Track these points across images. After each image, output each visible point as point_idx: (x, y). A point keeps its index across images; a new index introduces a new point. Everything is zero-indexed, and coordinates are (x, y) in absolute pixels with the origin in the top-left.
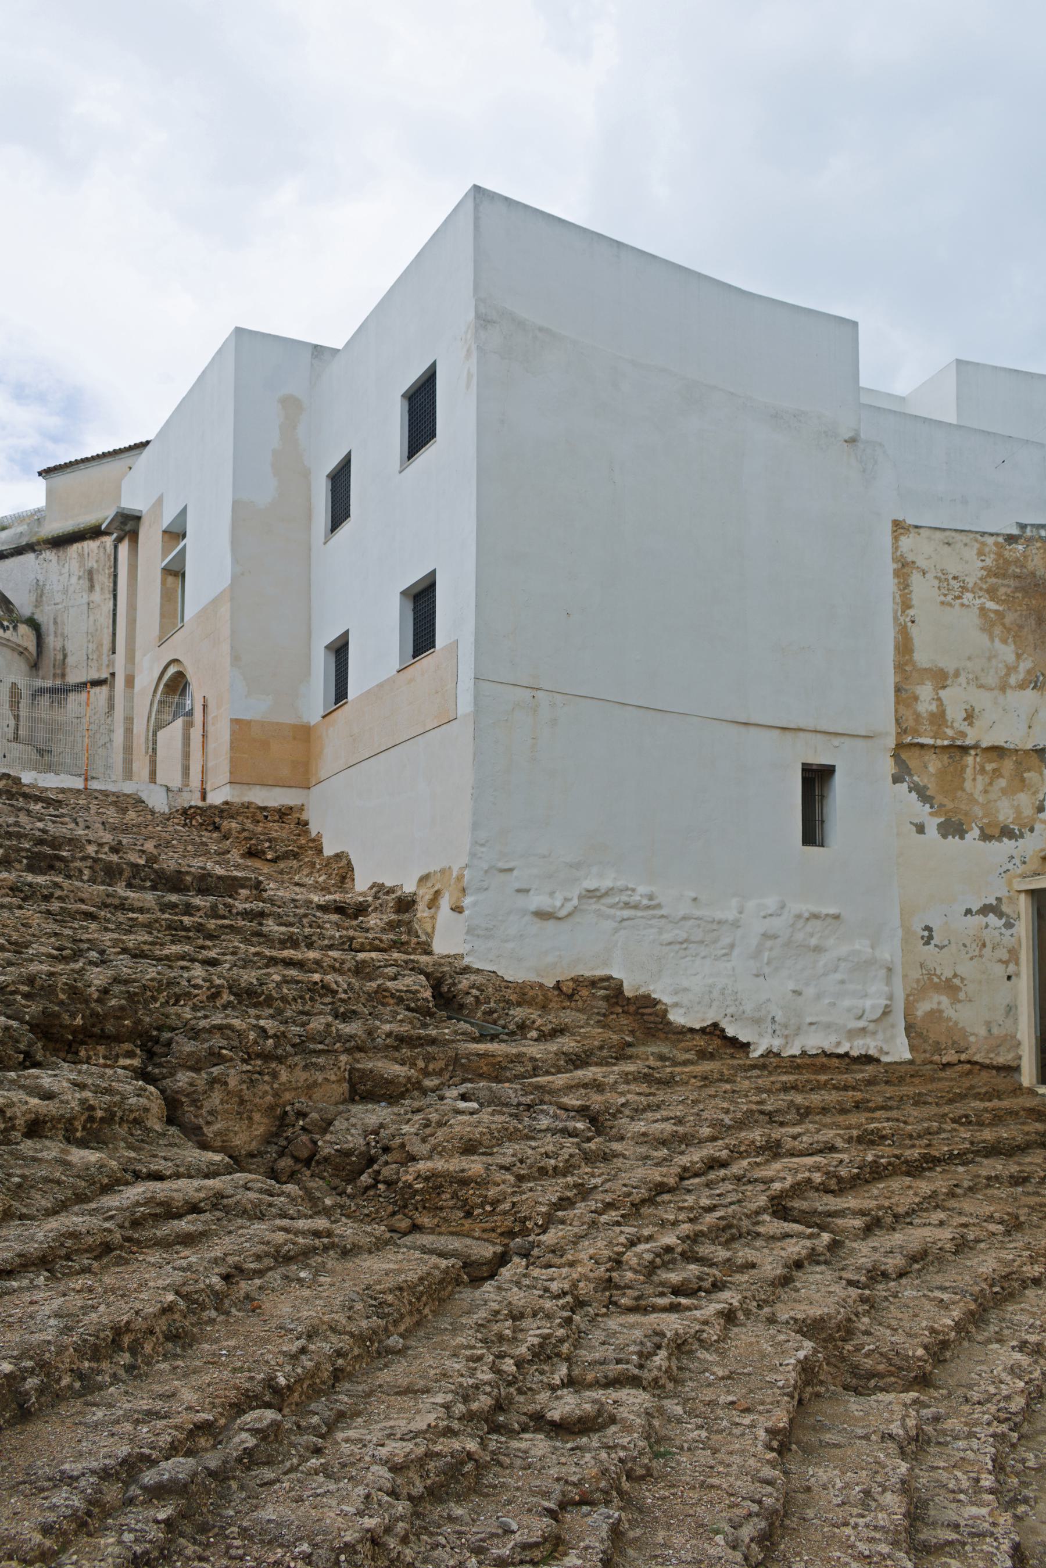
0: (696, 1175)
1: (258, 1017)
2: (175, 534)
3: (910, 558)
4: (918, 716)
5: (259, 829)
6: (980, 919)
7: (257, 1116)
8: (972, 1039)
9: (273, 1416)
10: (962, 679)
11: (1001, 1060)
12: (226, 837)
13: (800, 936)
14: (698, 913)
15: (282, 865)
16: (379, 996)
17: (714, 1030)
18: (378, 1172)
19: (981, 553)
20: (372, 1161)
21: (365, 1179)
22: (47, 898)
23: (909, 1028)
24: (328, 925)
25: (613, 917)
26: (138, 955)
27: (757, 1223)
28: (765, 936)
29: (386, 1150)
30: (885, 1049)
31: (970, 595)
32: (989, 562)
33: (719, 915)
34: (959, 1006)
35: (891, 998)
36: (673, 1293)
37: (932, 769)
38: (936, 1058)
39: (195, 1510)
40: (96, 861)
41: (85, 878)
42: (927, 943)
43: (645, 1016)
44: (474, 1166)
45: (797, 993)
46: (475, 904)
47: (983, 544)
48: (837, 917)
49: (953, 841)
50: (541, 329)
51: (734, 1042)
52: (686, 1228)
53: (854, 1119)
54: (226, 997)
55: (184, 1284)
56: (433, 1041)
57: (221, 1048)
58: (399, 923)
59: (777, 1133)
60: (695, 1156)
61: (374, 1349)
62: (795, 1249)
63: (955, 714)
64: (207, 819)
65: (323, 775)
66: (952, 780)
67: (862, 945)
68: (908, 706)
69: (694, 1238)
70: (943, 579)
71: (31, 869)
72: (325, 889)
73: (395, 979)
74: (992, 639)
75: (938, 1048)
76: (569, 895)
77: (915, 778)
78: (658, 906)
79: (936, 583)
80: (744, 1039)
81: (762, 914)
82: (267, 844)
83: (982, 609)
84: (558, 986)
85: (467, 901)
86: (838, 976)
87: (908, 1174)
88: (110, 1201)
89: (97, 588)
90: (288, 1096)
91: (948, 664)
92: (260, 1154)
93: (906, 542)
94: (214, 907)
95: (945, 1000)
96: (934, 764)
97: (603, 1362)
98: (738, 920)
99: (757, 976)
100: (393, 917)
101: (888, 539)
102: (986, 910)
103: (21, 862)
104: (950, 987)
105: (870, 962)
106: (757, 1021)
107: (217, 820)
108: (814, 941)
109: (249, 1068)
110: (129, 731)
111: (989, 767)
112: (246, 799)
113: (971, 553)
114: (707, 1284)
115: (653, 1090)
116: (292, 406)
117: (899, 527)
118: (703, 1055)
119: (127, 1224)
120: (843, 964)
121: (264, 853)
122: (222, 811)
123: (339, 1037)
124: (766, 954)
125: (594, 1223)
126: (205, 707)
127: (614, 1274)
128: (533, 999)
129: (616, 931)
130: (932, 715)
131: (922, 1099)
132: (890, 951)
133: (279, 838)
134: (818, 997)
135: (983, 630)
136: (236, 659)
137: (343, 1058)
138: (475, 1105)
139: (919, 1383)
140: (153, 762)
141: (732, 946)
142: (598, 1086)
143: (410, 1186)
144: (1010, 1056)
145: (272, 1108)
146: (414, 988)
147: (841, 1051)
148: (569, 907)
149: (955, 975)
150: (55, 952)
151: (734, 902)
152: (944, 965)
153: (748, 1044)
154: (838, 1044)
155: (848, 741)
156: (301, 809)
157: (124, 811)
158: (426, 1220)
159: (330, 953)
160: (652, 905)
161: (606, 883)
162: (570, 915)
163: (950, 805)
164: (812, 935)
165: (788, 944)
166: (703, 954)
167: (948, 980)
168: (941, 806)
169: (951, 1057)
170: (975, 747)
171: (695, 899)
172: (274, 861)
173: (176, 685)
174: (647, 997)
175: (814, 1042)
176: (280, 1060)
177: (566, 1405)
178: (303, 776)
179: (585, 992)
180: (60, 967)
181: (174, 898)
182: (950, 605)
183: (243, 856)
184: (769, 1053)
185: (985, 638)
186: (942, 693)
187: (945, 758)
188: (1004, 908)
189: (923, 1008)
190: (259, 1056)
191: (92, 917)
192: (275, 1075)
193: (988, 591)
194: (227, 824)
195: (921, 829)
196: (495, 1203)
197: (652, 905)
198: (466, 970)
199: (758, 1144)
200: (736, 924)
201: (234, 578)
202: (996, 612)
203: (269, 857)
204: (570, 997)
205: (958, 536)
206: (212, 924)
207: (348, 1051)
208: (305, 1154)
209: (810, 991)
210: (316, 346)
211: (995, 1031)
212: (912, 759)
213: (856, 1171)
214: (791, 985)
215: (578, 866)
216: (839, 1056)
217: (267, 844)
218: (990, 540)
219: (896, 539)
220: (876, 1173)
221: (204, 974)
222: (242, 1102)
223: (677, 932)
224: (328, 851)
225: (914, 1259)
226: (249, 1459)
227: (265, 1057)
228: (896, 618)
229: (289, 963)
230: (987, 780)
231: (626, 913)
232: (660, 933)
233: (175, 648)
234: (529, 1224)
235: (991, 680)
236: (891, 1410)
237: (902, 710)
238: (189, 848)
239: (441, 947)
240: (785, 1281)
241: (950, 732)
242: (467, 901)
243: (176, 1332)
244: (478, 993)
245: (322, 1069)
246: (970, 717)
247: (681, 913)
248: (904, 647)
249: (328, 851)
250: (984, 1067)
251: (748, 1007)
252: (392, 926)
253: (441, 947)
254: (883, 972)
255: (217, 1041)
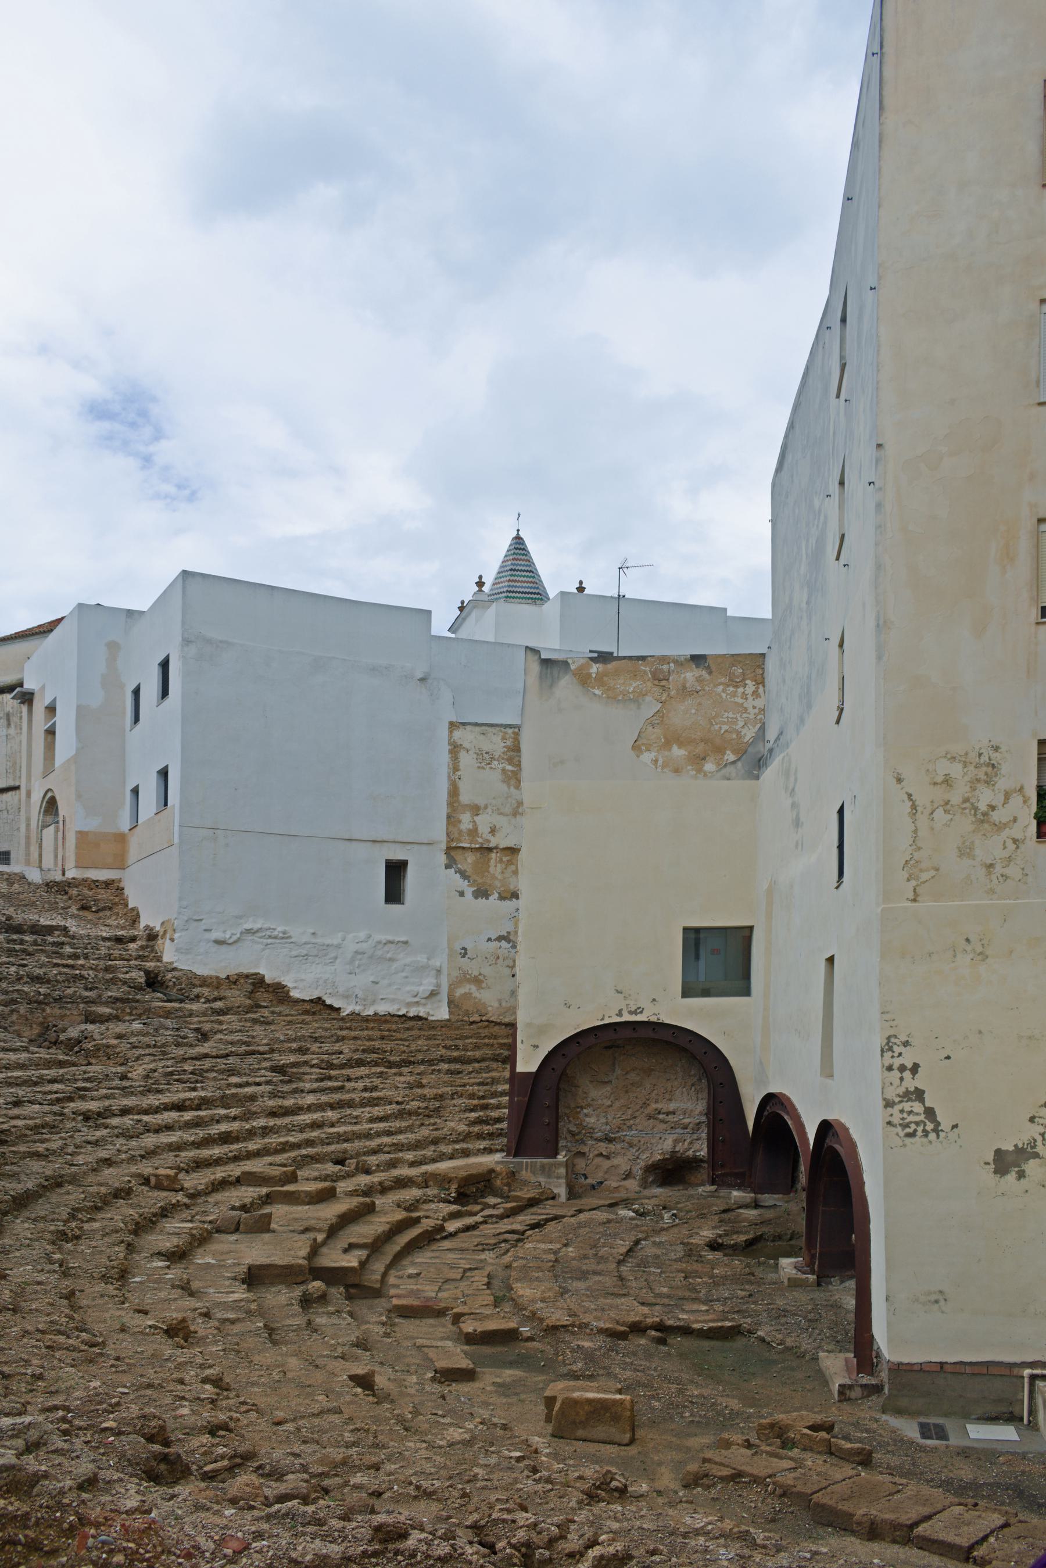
2: (51, 709)
3: (459, 742)
4: (460, 832)
5: (91, 894)
6: (496, 944)
7: (34, 1026)
8: (490, 1009)
10: (489, 810)
11: (506, 1020)
12: (70, 899)
13: (379, 953)
14: (314, 941)
15: (101, 914)
17: (319, 1000)
19: (503, 738)
20: (80, 1042)
21: (76, 1049)
23: (450, 1003)
25: (262, 943)
28: (357, 952)
29: (86, 1038)
30: (431, 1013)
31: (496, 763)
32: (508, 743)
33: (328, 941)
34: (482, 991)
35: (438, 986)
37: (469, 860)
38: (466, 1018)
42: (464, 957)
43: (279, 992)
46: (180, 937)
47: (506, 733)
48: (406, 943)
49: (482, 901)
50: (221, 642)
51: (331, 1007)
54: (26, 979)
56: (138, 1001)
58: (147, 946)
63: (484, 830)
64: (59, 888)
65: (130, 862)
66: (482, 867)
67: (422, 959)
68: (454, 826)
70: (480, 754)
72: (123, 928)
73: (127, 973)
74: (509, 787)
75: (467, 1013)
78: (290, 937)
79: (475, 756)
80: (336, 1006)
83: (504, 770)
84: (228, 977)
85: (176, 936)
86: (404, 974)
89: (13, 726)
90: (51, 1019)
91: (481, 801)
92: (35, 1040)
93: (457, 734)
94: (35, 941)
95: (473, 988)
96: (471, 858)
99: (350, 973)
101: (446, 732)
102: (500, 938)
104: (477, 981)
105: (425, 967)
106: (347, 997)
108: (389, 956)
110: (28, 825)
111: (505, 859)
112: (86, 876)
113: (497, 739)
116: (113, 647)
117: (453, 726)
120: (407, 968)
123: (80, 997)
128: (211, 983)
129: (264, 950)
130: (470, 830)
132: (440, 960)
133: (102, 898)
135: (503, 782)
136: (79, 796)
137: (82, 1006)
140: (40, 847)
141: (336, 958)
144: (512, 1018)
145: (42, 1023)
147: (400, 1013)
148: (235, 938)
149: (480, 974)
151: (340, 935)
152: (473, 968)
153: (340, 1009)
154: (399, 1010)
155: (416, 846)
156: (120, 880)
157: (11, 884)
158: (93, 1061)
160: (285, 936)
161: (258, 926)
162: (235, 942)
163: (480, 881)
164: (388, 952)
165: (371, 957)
168: (475, 881)
169: (476, 1018)
170: (496, 848)
171: (313, 934)
172: (97, 912)
173: (51, 805)
174: (279, 984)
175: (383, 1008)
176: (46, 1004)
178: (121, 864)
179: (242, 981)
181: (15, 937)
182: (483, 768)
183: (78, 909)
184: (353, 1013)
185: (504, 787)
186: (476, 818)
187: (478, 855)
188: (512, 937)
189: (459, 992)
190: (35, 1002)
192: (44, 1010)
193: (507, 760)
194: (74, 892)
195: (462, 894)
196: (118, 1053)
197: (285, 936)
198: (174, 969)
200: (338, 946)
201: (77, 750)
202: (512, 771)
204: (235, 983)
205: (490, 729)
206: (31, 949)
207: (86, 1003)
208: (53, 1040)
210: (129, 611)
211: (504, 1004)
212: (458, 856)
214: (372, 979)
215: (240, 917)
216: (399, 1016)
218: (510, 731)
219: (451, 732)
222: (27, 1019)
224: (130, 906)
227: (40, 1003)
228: (449, 777)
230: (504, 866)
231: (270, 941)
233: (50, 782)
235: (508, 810)
237: (451, 828)
238: (46, 906)
239: (166, 958)
241: (480, 840)
242: (176, 936)
245: (69, 1009)
246: (493, 831)
247: (304, 941)
248: (454, 792)
249: (130, 906)
250: (497, 1024)
251: (341, 990)
252: (142, 948)
254: (434, 972)
255: (15, 995)
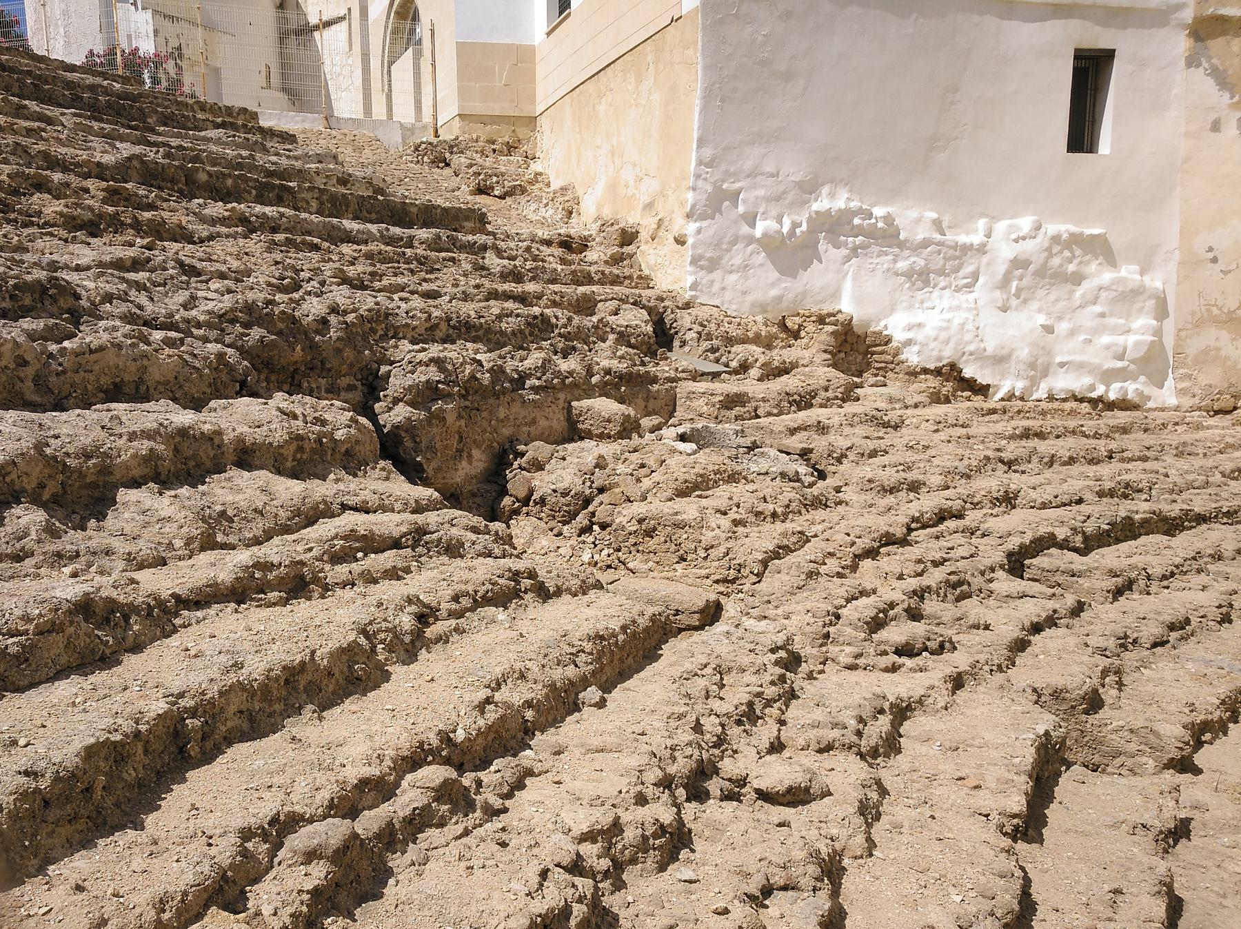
0: (924, 527)
1: (477, 352)
9: (447, 775)
16: (600, 332)
18: (593, 514)
20: (587, 501)
22: (274, 230)
24: (551, 259)
26: (358, 285)
27: (991, 581)
33: (963, 239)
36: (895, 653)
39: (358, 875)
40: (322, 191)
41: (314, 210)
44: (689, 508)
45: (1049, 329)
52: (913, 583)
53: (1105, 470)
55: (371, 623)
57: (439, 382)
59: (1016, 481)
60: (927, 503)
61: (562, 703)
62: (1032, 610)
67: (1128, 272)
69: (920, 594)
71: (261, 200)
76: (797, 218)
77: (1215, 61)
80: (982, 380)
81: (1014, 236)
82: (495, 179)
86: (1098, 309)
87: (1167, 533)
88: (312, 533)
97: (817, 725)
98: (984, 245)
100: (616, 249)
103: (250, 193)
105: (1137, 292)
107: (448, 155)
108: (1071, 268)
109: (467, 403)
114: (933, 645)
115: (881, 434)
118: (937, 398)
119: (325, 558)
120: (1104, 295)
121: (493, 188)
122: (451, 147)
123: (557, 374)
124: (1014, 284)
125: (811, 575)
126: (432, 31)
127: (832, 629)
131: (1188, 449)
134: (1072, 333)
138: (694, 446)
139: (1174, 767)
142: (822, 429)
143: (623, 528)
146: (634, 323)
147: (1094, 395)
150: (275, 281)
159: (551, 286)
166: (942, 284)
167: (1231, 312)
177: (776, 773)
180: (279, 297)
181: (396, 231)
184: (1010, 397)
191: (316, 248)
199: (995, 495)
200: (982, 249)
203: (497, 193)
209: (1063, 327)
213: (1107, 527)
214: (1041, 319)
217: (495, 179)
220: (1126, 530)
221: (422, 305)
223: (913, 259)
225: (1172, 627)
226: (418, 822)
229: (508, 296)
232: (895, 261)
234: (745, 572)
236: (1140, 795)
240: (1020, 646)
243: (350, 674)
244: (700, 329)
247: (920, 237)
253: (663, 283)
